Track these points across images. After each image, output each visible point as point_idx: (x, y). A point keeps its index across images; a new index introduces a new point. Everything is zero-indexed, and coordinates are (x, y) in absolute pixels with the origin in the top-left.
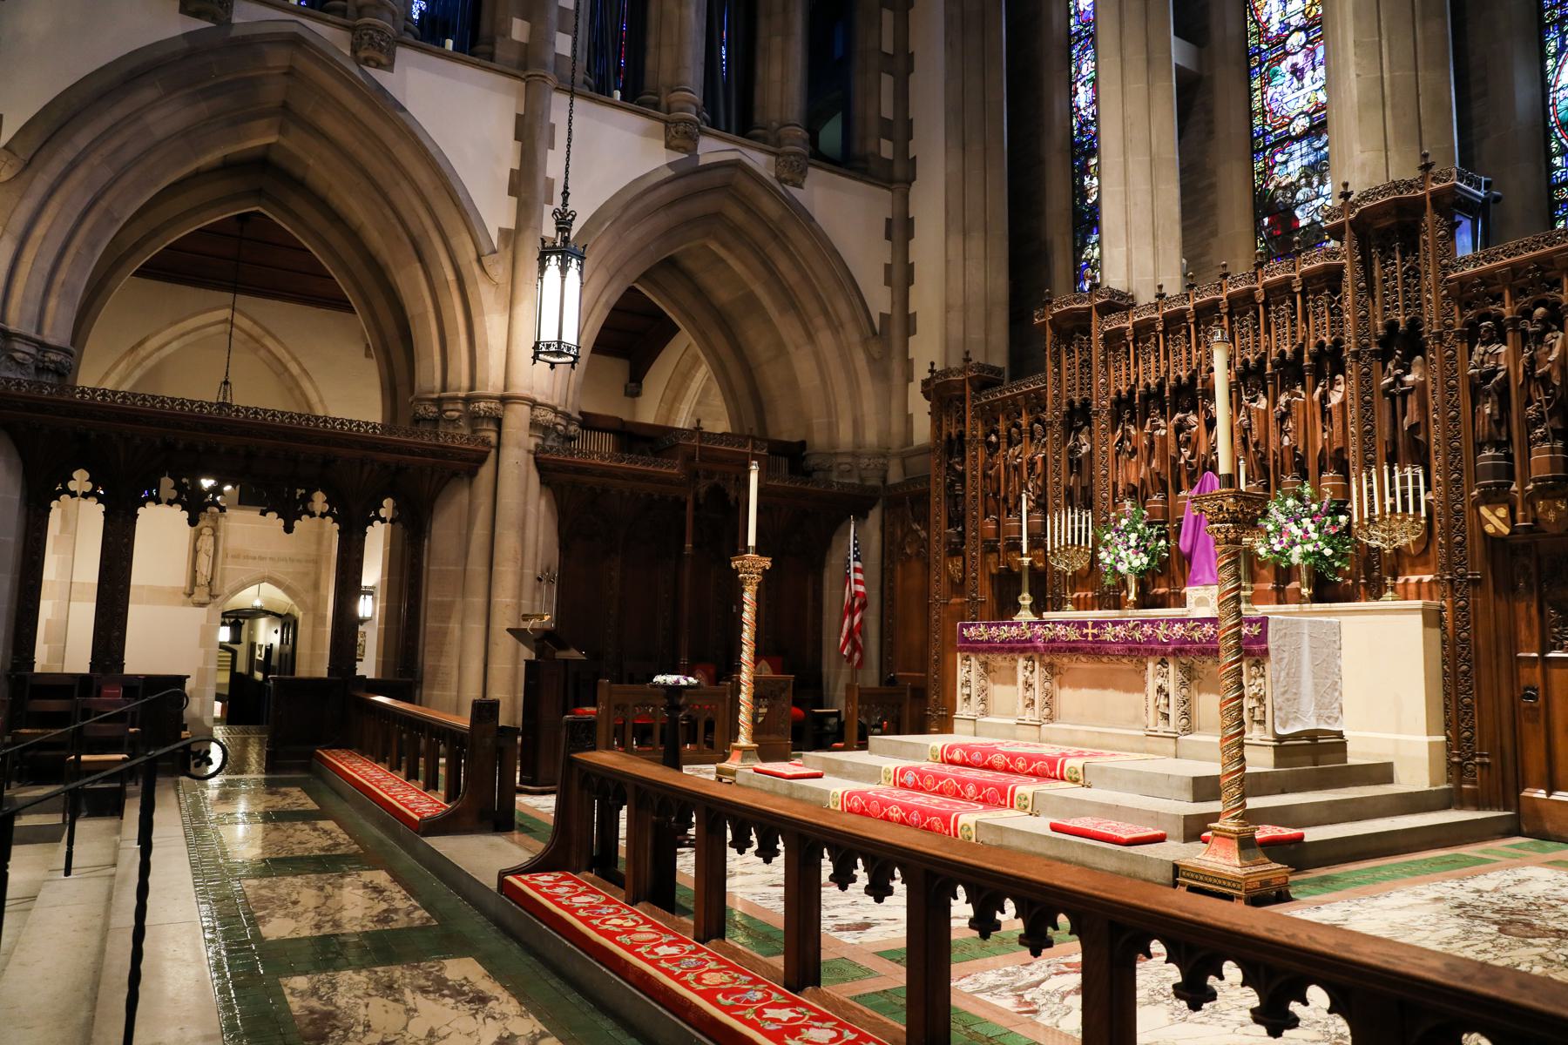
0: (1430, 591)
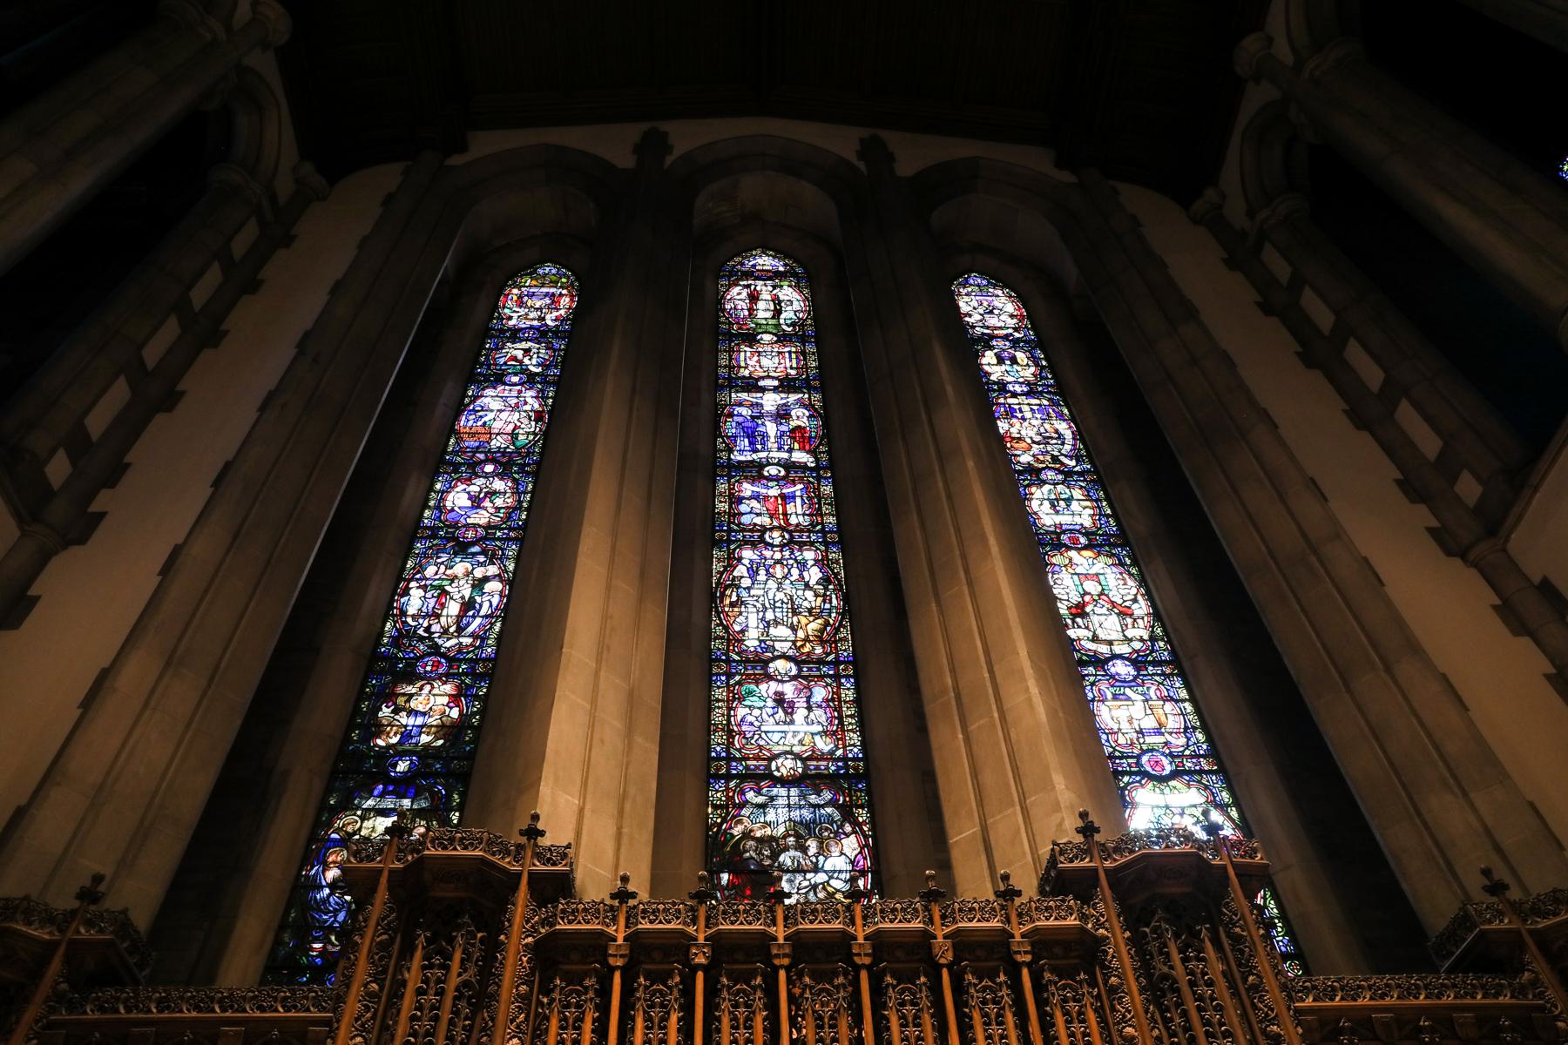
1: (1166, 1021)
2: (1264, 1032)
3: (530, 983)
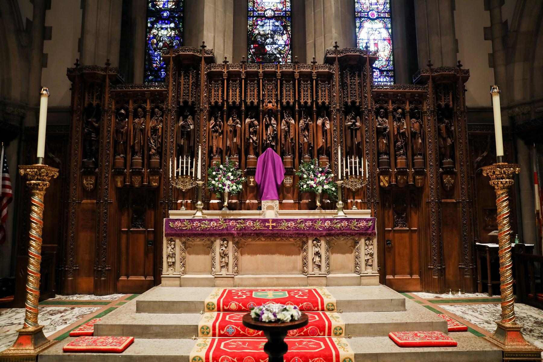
0: (361, 206)
1: (344, 92)
2: (364, 95)
3: (207, 82)
